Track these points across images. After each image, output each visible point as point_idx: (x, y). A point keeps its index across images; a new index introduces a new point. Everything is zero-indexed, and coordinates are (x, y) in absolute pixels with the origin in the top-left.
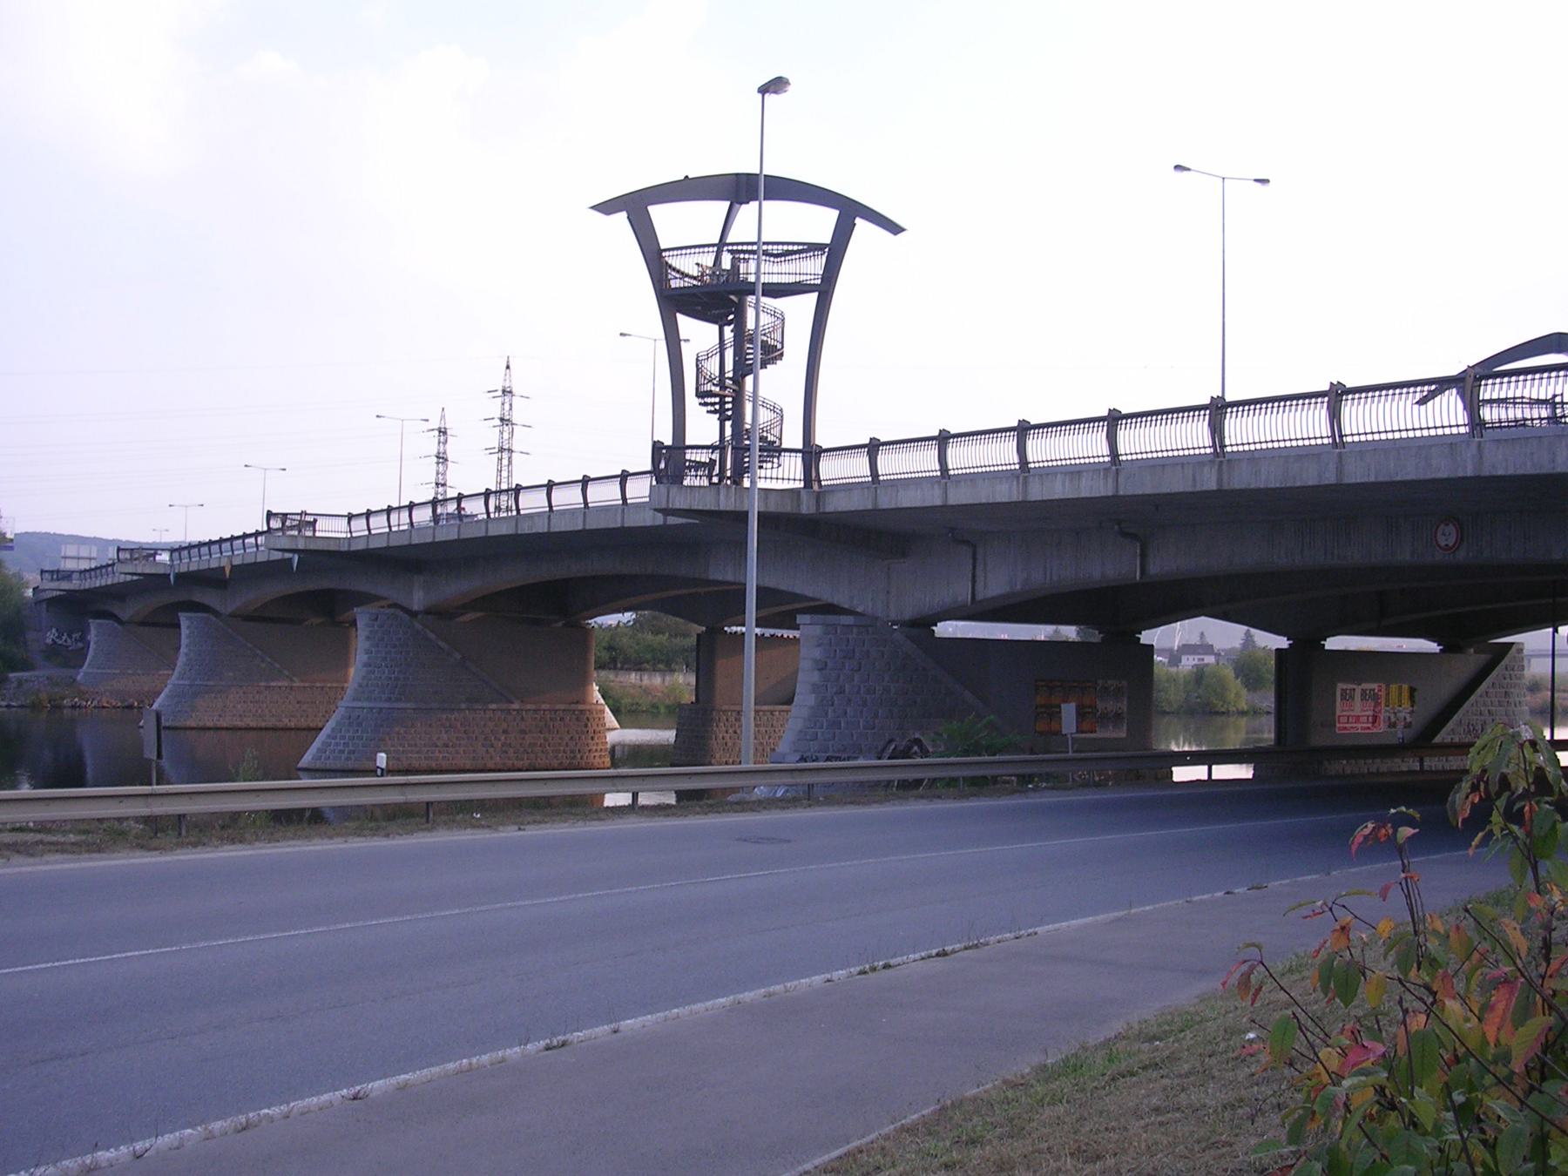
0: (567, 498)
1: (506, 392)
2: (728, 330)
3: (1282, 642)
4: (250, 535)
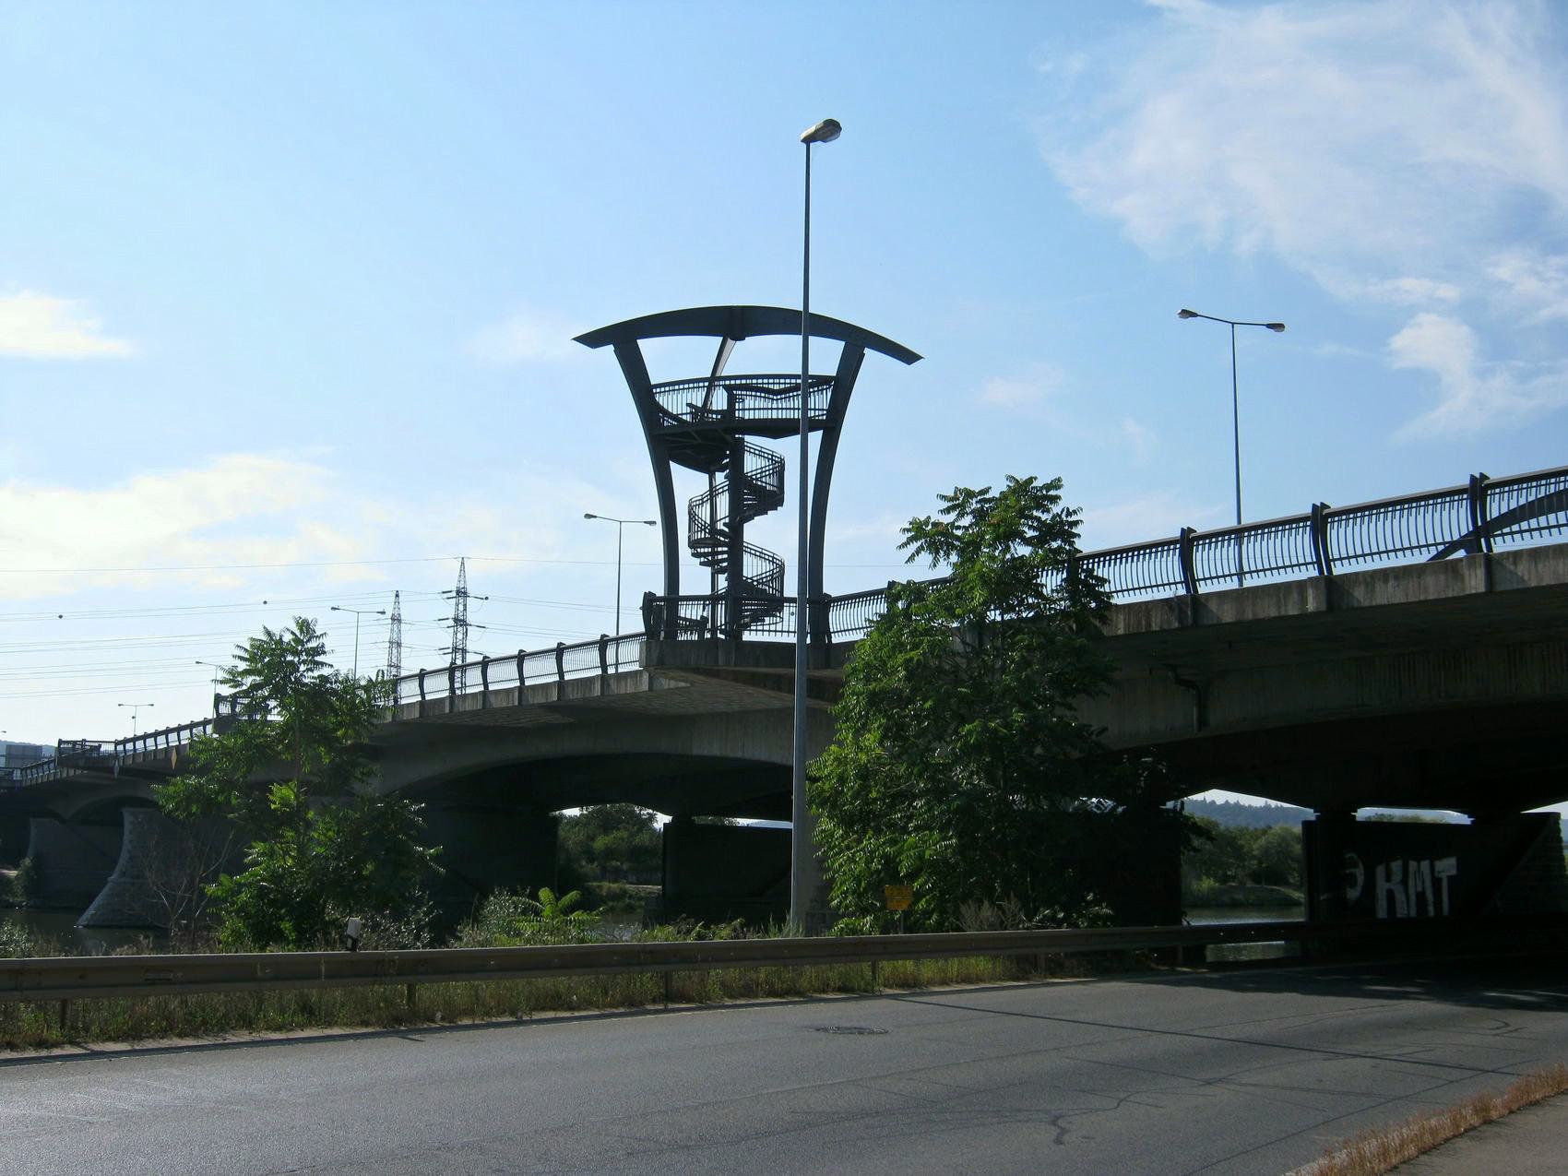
0: (541, 673)
1: (462, 593)
2: (720, 477)
3: (1310, 814)
4: (198, 724)
